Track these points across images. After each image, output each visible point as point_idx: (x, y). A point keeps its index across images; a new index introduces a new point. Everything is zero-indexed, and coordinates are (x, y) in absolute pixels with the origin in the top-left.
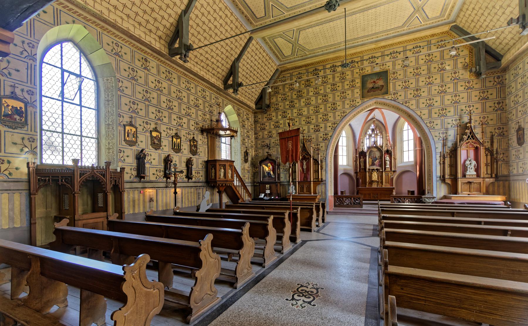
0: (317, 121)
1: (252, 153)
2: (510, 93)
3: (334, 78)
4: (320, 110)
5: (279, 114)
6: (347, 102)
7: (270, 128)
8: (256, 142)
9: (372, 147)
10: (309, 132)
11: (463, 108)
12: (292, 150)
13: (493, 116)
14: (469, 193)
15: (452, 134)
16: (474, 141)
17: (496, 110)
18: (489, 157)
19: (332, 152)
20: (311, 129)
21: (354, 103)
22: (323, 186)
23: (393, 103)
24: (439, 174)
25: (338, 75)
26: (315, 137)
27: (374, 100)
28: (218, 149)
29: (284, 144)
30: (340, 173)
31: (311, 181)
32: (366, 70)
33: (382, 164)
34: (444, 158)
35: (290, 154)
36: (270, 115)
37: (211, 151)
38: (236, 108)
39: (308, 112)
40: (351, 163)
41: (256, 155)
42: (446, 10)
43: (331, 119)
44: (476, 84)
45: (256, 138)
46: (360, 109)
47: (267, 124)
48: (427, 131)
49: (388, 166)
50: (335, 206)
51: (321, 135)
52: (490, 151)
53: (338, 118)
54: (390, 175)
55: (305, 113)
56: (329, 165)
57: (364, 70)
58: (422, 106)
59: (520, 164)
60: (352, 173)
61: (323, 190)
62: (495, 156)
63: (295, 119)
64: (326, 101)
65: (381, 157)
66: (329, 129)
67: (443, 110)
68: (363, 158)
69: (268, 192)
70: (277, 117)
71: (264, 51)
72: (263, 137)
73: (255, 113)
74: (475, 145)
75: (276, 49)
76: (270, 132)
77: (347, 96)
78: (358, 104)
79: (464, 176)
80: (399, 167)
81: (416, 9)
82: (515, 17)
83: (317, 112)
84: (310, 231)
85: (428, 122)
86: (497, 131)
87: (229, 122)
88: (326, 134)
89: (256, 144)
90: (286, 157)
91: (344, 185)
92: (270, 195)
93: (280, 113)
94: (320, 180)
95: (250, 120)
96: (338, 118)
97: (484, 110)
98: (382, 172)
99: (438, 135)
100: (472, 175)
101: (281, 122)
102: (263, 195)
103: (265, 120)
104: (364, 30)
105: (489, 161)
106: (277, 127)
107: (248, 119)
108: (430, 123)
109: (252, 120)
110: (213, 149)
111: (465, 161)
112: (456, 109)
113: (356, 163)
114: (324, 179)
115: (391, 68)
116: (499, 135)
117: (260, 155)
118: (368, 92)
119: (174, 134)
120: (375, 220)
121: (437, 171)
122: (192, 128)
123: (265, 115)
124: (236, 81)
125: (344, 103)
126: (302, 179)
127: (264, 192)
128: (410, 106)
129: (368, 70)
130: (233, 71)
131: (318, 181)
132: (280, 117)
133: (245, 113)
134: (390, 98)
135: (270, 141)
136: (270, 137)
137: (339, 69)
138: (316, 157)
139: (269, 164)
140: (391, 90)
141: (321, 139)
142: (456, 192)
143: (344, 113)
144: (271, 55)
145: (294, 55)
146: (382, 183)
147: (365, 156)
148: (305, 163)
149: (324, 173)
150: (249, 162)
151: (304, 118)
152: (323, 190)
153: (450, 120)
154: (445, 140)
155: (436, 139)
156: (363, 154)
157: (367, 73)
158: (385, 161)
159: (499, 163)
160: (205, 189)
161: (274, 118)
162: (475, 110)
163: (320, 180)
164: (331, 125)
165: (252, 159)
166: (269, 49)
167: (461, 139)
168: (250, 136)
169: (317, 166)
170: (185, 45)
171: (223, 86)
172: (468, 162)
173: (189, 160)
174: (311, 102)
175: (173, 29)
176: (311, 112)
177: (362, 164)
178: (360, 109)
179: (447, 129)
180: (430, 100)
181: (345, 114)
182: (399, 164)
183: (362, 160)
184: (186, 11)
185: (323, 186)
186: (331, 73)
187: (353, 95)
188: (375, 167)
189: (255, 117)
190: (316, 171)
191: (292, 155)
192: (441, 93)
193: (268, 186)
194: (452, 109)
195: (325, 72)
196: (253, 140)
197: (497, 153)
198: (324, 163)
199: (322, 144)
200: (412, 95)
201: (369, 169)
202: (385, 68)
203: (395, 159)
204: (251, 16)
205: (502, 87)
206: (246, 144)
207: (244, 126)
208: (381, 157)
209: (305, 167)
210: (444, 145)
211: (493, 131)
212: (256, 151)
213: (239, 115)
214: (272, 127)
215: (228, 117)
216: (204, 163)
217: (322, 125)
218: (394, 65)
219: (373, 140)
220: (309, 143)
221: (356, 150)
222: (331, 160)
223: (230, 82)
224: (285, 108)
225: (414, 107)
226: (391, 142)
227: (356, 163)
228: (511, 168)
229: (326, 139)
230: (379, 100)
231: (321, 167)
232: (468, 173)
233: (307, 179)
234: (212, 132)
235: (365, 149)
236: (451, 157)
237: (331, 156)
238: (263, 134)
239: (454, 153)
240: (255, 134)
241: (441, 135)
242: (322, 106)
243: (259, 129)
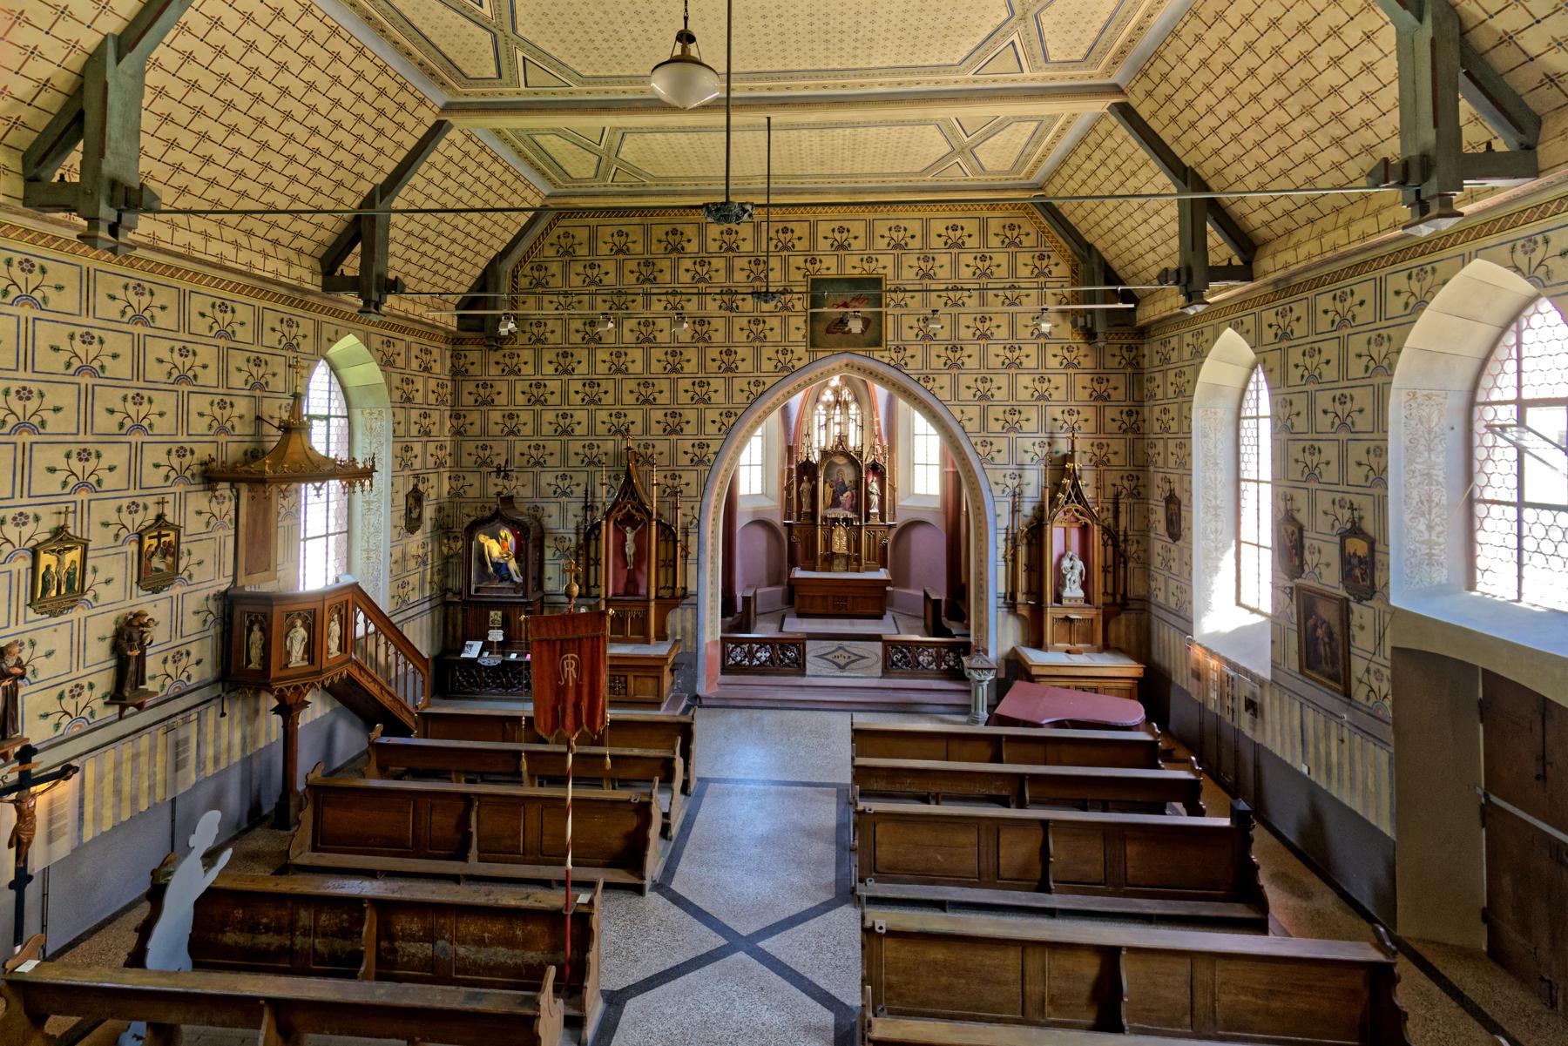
0: (674, 399)
1: (437, 489)
2: (1152, 396)
3: (730, 270)
4: (685, 364)
5: (546, 358)
6: (768, 352)
7: (512, 401)
8: (458, 447)
9: (835, 452)
10: (646, 430)
11: (1059, 416)
12: (578, 688)
13: (1118, 445)
14: (1068, 646)
15: (1034, 480)
16: (1080, 507)
17: (1125, 431)
18: (1110, 549)
19: (719, 501)
20: (654, 425)
21: (789, 356)
22: (689, 613)
23: (894, 374)
24: (1002, 589)
25: (743, 262)
26: (666, 451)
27: (845, 359)
28: (283, 524)
29: (545, 658)
30: (741, 521)
31: (648, 600)
32: (824, 265)
33: (860, 504)
34: (1015, 547)
35: (571, 698)
36: (511, 356)
37: (251, 543)
38: (376, 341)
39: (647, 364)
40: (776, 489)
41: (455, 494)
42: (1025, 163)
43: (718, 398)
44: (1084, 355)
45: (458, 432)
46: (806, 377)
47: (502, 386)
48: (976, 466)
49: (875, 510)
50: (726, 670)
51: (687, 445)
52: (1111, 534)
53: (739, 398)
54: (879, 535)
55: (637, 368)
56: (709, 543)
57: (817, 266)
58: (966, 395)
59: (1173, 584)
60: (778, 520)
61: (689, 626)
62: (1122, 546)
63: (603, 383)
64: (705, 340)
65: (858, 483)
66: (711, 429)
67: (1013, 412)
68: (809, 481)
69: (496, 636)
70: (537, 366)
71: (495, 159)
72: (484, 431)
73: (455, 341)
74: (1083, 519)
75: (541, 159)
76: (511, 416)
77: (768, 333)
78: (798, 365)
79: (1058, 599)
80: (905, 508)
81: (958, 149)
82: (1173, 264)
83: (674, 370)
84: (639, 890)
85: (979, 441)
86: (1126, 483)
87: (344, 389)
88: (701, 446)
89: (456, 454)
90: (555, 709)
91: (753, 551)
92: (504, 647)
93: (548, 355)
94: (679, 592)
95: (436, 368)
96: (739, 398)
97: (1100, 428)
98: (860, 527)
99: (1001, 480)
100: (1076, 599)
101: (554, 385)
102: (478, 645)
103: (494, 371)
104: (822, 163)
105: (1110, 562)
106: (538, 401)
107: (427, 369)
108: (984, 444)
109: (441, 367)
110: (259, 540)
111: (1061, 557)
112: (1042, 417)
113: (789, 493)
114: (692, 588)
115: (890, 272)
116: (1131, 495)
117: (472, 493)
118: (828, 331)
119: (42, 538)
120: (839, 761)
121: (996, 579)
122: (153, 477)
123: (497, 356)
124: (376, 269)
125: (757, 353)
126: (621, 585)
127: (482, 636)
128: (937, 391)
129: (829, 266)
130: (362, 229)
131: (673, 597)
132: (549, 369)
133: (415, 350)
134: (886, 360)
135: (510, 449)
136: (511, 432)
137: (748, 304)
138: (667, 516)
139: (505, 532)
140: (890, 337)
141: (686, 460)
142: (1039, 644)
143: (757, 384)
144: (523, 170)
145: (605, 179)
146: (858, 560)
147: (814, 478)
148: (630, 536)
149: (692, 569)
150: (427, 524)
151: (632, 385)
152: (689, 626)
153: (1027, 444)
154: (1017, 495)
155: (997, 490)
156: (807, 470)
157: (824, 274)
158: (868, 493)
159: (1130, 565)
160: (212, 713)
161: (528, 370)
162: (1082, 424)
163: (679, 592)
164: (717, 418)
165: (440, 509)
166: (515, 156)
167: (1053, 499)
168: (435, 430)
169: (671, 544)
170: (114, 184)
171: (319, 280)
172: (1066, 563)
173: (129, 623)
174: (658, 335)
175: (52, 101)
176: (656, 367)
177: (806, 500)
178: (806, 377)
179: (1021, 467)
180: (984, 380)
181: (760, 389)
182: (902, 502)
183: (805, 486)
184: (128, 40)
185: (689, 613)
186: (723, 312)
187: (785, 334)
188: (840, 513)
189: (455, 356)
190: (669, 564)
191: (577, 706)
192: (1009, 366)
193: (496, 615)
194: (1033, 414)
195: (702, 306)
196: (447, 439)
197: (1126, 540)
198: (692, 539)
199: (690, 477)
200: (943, 360)
201: (825, 519)
202: (874, 269)
203: (893, 489)
204: (442, 67)
205: (1137, 374)
206: (417, 464)
207: (409, 400)
208: (858, 483)
209: (630, 549)
210: (1015, 510)
211: (1118, 482)
212: (458, 417)
213: (386, 364)
214: (521, 399)
215: (337, 397)
216: (212, 605)
217: (691, 415)
218: (898, 266)
219: (837, 430)
220: (647, 468)
221: (790, 449)
222: (715, 536)
223: (351, 266)
224: (567, 340)
225: (945, 395)
226: (885, 442)
227: (789, 493)
228: (1153, 585)
229: (701, 461)
230: (857, 360)
231: (685, 548)
232: (1067, 593)
233: (637, 587)
234: (261, 470)
235: (816, 458)
236: (1029, 544)
237: (716, 513)
238: (485, 419)
239: (1036, 533)
240: (456, 416)
241: (1009, 482)
242: (691, 354)
243: (468, 400)
